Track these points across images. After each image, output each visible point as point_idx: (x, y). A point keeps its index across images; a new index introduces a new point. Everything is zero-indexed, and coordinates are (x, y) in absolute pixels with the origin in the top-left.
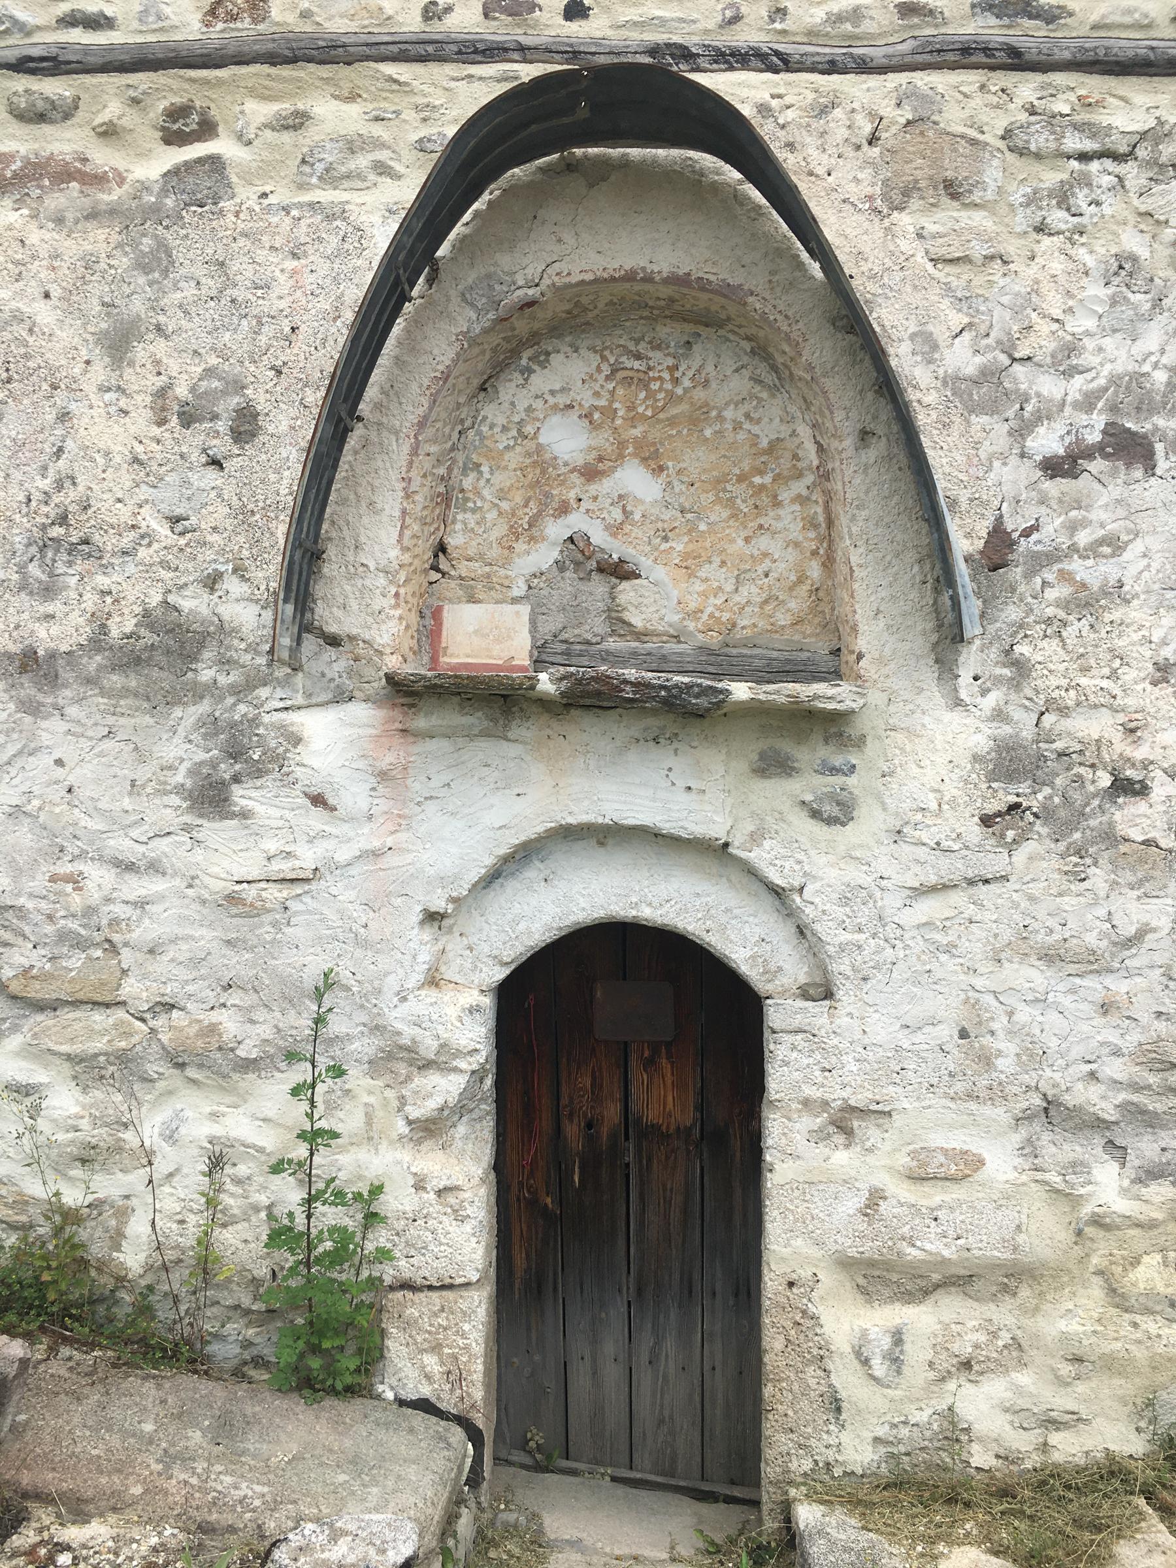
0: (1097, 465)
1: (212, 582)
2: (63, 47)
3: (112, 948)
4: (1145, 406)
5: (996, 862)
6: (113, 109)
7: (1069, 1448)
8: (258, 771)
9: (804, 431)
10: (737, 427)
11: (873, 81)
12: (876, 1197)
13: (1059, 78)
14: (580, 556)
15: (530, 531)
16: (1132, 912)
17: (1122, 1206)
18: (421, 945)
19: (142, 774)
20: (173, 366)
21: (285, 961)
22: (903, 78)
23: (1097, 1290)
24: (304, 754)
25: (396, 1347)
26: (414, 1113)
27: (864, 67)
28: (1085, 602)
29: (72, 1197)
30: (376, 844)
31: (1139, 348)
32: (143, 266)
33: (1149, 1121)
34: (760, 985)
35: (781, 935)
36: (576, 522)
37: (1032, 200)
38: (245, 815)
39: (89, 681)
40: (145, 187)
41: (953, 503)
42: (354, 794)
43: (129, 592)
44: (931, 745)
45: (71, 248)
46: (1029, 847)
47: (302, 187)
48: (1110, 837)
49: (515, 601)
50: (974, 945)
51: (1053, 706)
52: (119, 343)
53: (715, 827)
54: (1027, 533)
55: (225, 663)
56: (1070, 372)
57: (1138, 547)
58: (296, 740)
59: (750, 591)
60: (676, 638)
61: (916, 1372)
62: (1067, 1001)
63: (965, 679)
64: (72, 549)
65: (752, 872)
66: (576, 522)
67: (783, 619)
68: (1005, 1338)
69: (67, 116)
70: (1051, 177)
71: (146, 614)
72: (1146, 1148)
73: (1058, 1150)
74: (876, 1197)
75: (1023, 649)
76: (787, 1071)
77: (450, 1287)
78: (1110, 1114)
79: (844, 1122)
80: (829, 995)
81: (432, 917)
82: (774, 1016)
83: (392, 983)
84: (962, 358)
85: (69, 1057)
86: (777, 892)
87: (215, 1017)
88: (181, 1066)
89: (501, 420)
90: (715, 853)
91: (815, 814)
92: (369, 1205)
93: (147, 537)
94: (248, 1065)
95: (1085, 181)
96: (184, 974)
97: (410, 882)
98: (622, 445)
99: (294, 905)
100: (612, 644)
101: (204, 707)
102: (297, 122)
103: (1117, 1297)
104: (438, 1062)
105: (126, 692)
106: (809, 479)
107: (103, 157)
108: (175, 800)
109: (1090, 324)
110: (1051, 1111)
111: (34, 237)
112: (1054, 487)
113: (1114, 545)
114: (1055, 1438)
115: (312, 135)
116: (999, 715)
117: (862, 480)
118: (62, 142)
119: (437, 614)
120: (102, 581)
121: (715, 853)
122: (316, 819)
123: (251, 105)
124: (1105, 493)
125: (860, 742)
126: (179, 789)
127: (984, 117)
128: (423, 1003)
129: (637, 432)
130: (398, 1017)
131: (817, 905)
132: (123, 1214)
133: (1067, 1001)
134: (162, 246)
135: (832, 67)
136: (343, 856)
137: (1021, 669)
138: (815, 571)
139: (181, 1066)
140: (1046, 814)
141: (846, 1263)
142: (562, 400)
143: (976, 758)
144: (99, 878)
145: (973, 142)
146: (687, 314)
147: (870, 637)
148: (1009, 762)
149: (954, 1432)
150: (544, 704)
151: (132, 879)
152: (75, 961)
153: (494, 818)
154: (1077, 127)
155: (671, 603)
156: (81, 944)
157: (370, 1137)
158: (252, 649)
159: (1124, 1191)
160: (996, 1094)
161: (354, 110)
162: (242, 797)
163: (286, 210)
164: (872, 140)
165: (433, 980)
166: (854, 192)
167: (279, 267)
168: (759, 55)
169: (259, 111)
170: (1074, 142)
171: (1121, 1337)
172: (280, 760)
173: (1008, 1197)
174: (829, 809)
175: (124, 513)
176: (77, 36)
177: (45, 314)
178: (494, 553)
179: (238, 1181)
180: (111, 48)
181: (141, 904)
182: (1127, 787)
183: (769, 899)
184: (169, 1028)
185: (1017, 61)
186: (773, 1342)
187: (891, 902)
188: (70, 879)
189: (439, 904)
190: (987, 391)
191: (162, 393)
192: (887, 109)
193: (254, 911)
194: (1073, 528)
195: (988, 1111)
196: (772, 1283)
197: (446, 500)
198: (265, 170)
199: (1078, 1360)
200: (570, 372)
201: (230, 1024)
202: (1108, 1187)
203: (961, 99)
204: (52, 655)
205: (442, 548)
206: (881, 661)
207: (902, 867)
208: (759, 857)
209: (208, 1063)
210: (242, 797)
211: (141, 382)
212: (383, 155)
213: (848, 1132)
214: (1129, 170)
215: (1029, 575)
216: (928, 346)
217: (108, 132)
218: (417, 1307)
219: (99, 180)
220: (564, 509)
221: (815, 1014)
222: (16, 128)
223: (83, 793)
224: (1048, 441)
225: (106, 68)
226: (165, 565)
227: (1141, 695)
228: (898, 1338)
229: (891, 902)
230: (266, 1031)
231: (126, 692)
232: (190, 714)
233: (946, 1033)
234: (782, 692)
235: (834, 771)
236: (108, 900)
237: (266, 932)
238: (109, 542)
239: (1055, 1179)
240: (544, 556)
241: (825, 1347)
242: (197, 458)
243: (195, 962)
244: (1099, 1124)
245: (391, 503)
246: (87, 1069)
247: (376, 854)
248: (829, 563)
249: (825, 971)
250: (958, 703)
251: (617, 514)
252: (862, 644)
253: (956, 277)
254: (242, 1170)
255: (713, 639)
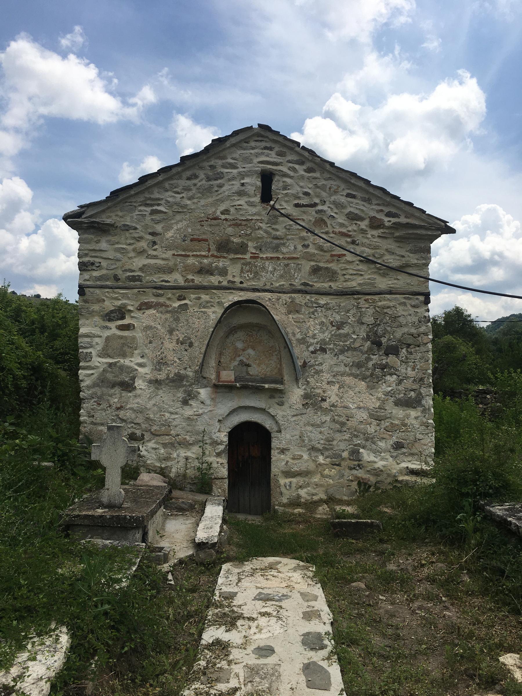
0: (319, 352)
1: (185, 369)
2: (162, 285)
3: (169, 426)
4: (326, 344)
5: (304, 411)
6: (170, 295)
7: (315, 498)
8: (193, 398)
9: (277, 344)
10: (266, 343)
11: (286, 295)
12: (287, 462)
13: (313, 295)
14: (242, 363)
15: (234, 359)
16: (324, 418)
17: (323, 462)
18: (217, 425)
19: (174, 399)
20: (180, 335)
21: (197, 428)
22: (290, 295)
23: (319, 475)
24: (200, 395)
25: (214, 488)
26: (217, 451)
27: (284, 293)
28: (318, 372)
29: (163, 466)
30: (211, 409)
31: (325, 335)
32: (175, 320)
33: (327, 449)
34: (271, 431)
35: (273, 423)
36: (241, 358)
37: (309, 313)
38: (191, 405)
39: (167, 384)
40: (175, 308)
41: (298, 358)
42: (208, 402)
43: (173, 370)
44: (296, 394)
45: (164, 317)
46: (309, 409)
47: (200, 308)
48: (321, 407)
49: (232, 370)
50: (301, 424)
51: (313, 388)
52: (171, 332)
53: (264, 407)
54: (309, 362)
55: (187, 381)
56: (315, 339)
57: (325, 364)
58: (199, 393)
59: (269, 369)
60: (257, 376)
61: (293, 488)
62: (315, 432)
63: (300, 384)
64: (164, 364)
65: (269, 413)
66: (241, 358)
67: (274, 373)
68: (306, 483)
69: (162, 296)
70: (311, 310)
71: (175, 374)
72: (327, 453)
73: (314, 454)
74: (287, 462)
75: (308, 379)
76: (274, 443)
77: (223, 479)
78: (321, 449)
79: (283, 451)
80: (280, 432)
81: (219, 421)
82: (272, 436)
83: (213, 431)
84: (299, 336)
85: (162, 443)
86: (273, 416)
87: (185, 437)
88: (180, 445)
89: (229, 342)
90: (263, 411)
91: (278, 404)
92: (210, 465)
93: (176, 362)
94: (191, 444)
95: (316, 311)
96: (181, 430)
97: (213, 417)
98: (248, 346)
99: (199, 419)
100: (247, 377)
101: (184, 388)
102: (199, 298)
103: (323, 476)
104: (221, 443)
105: (172, 386)
106: (277, 352)
107: (168, 303)
108: (180, 403)
109: (317, 332)
110: (313, 449)
111: (157, 315)
112: (312, 355)
113: (321, 364)
114: (313, 497)
115: (202, 300)
116: (305, 389)
117: (284, 353)
118: (161, 300)
119: (219, 372)
120: (168, 368)
121: (263, 411)
122: (202, 406)
123: (192, 295)
124: (320, 357)
125: (285, 393)
126: (180, 401)
127: (302, 301)
128: (218, 434)
129: (251, 344)
130: (214, 437)
131: (279, 418)
132: (171, 468)
133: (315, 432)
134: (178, 317)
135: (280, 293)
136: (206, 411)
137: (308, 382)
138: (279, 366)
139: (180, 445)
140: (312, 404)
141: (283, 472)
142: (239, 339)
143: (302, 396)
144: (167, 415)
145: (300, 305)
146: (259, 327)
147: (286, 378)
148: (306, 396)
149: (299, 497)
150: (238, 388)
151: (173, 415)
152: (163, 428)
153: (229, 405)
154: (315, 303)
155: (255, 370)
156: (164, 425)
157: (210, 456)
158: (192, 379)
159: (323, 460)
160: (305, 446)
161: (208, 296)
162: (191, 402)
163: (197, 312)
164: (286, 304)
165: (219, 431)
166: (283, 311)
167: (197, 321)
168: (269, 290)
169: (193, 296)
170: (315, 305)
171: (323, 481)
172: (196, 396)
173: (307, 461)
174: (280, 403)
175: (172, 358)
176: (164, 283)
177: (159, 327)
178: (228, 362)
179: (189, 463)
180: (169, 286)
181: (174, 419)
182: (324, 400)
183: (272, 417)
184: (178, 439)
185: (306, 292)
186: (272, 484)
187: (289, 417)
188: (163, 415)
189: (221, 418)
190: (303, 341)
191: (178, 340)
192: (288, 300)
193: (192, 420)
194: (315, 361)
195: (303, 448)
196: (272, 475)
197: (221, 354)
198: (194, 306)
199: (317, 485)
200: (240, 334)
201: (188, 438)
202: (321, 459)
203: (299, 298)
204: (160, 380)
205: (220, 361)
206: (288, 381)
207: (289, 412)
208: (270, 411)
209: (185, 444)
210: (191, 402)
211: (175, 338)
212: (212, 304)
213: (283, 452)
214: (323, 309)
215: (309, 368)
216: (294, 334)
217: (169, 299)
218: (217, 482)
219: (168, 306)
220: (239, 356)
221: (278, 435)
222: (154, 297)
223: (165, 402)
224: (311, 349)
225: (169, 289)
226: (178, 366)
227: (326, 386)
228: (291, 483)
229: (289, 417)
230: (193, 439)
231: (172, 386)
232: (182, 390)
233: (298, 437)
234: (273, 386)
235: (281, 398)
236: (169, 418)
237: (194, 423)
238: (169, 363)
239: (313, 458)
240: (236, 363)
241: (280, 485)
242: (183, 350)
243: (182, 428)
244: (320, 450)
245: (213, 357)
246: (165, 445)
247: (211, 411)
248: (281, 365)
249: (280, 428)
250: (299, 388)
251: (248, 356)
252: (285, 378)
253: (298, 324)
254: (190, 461)
255: (263, 376)
